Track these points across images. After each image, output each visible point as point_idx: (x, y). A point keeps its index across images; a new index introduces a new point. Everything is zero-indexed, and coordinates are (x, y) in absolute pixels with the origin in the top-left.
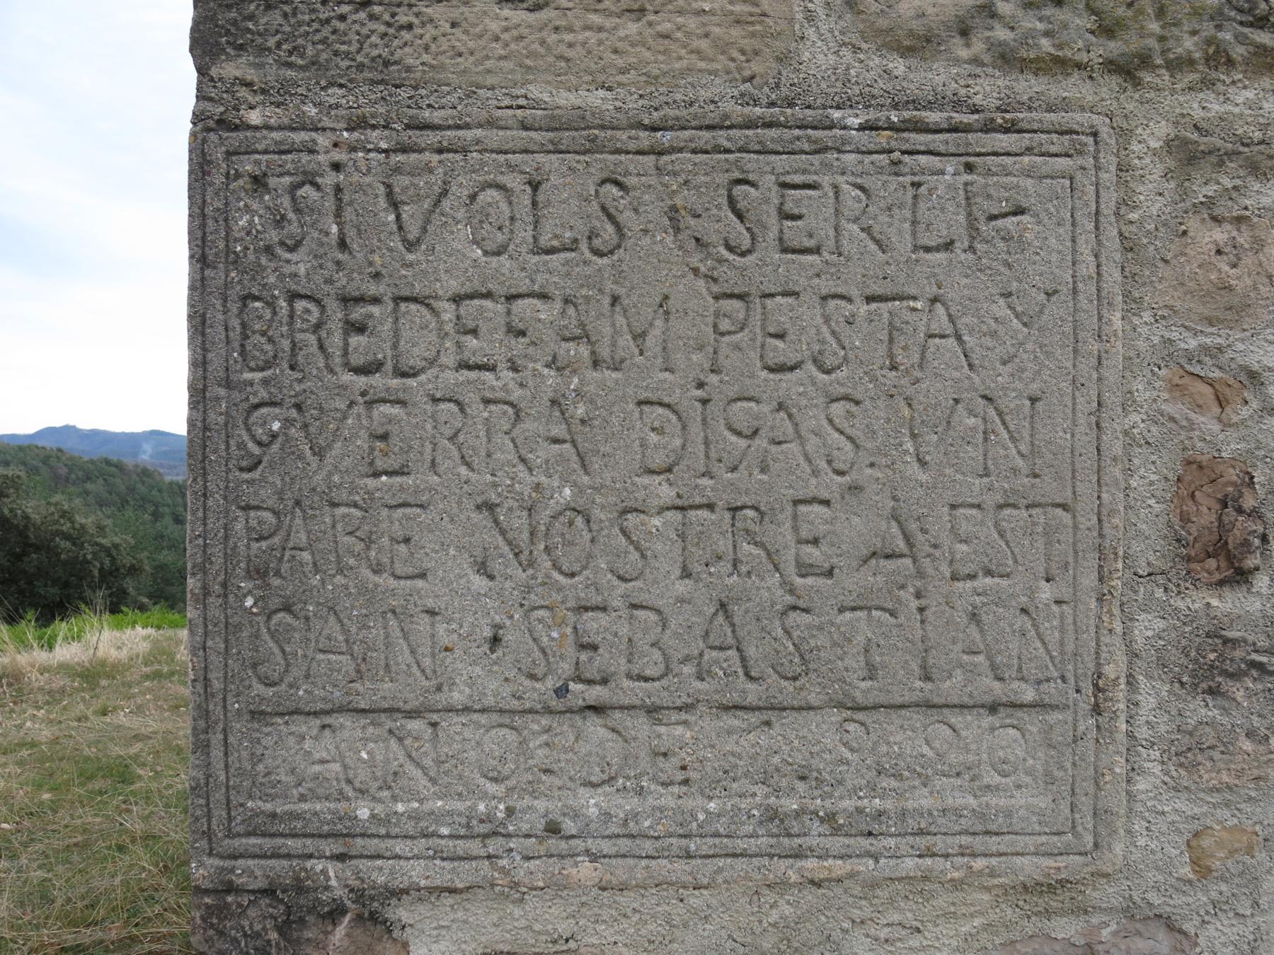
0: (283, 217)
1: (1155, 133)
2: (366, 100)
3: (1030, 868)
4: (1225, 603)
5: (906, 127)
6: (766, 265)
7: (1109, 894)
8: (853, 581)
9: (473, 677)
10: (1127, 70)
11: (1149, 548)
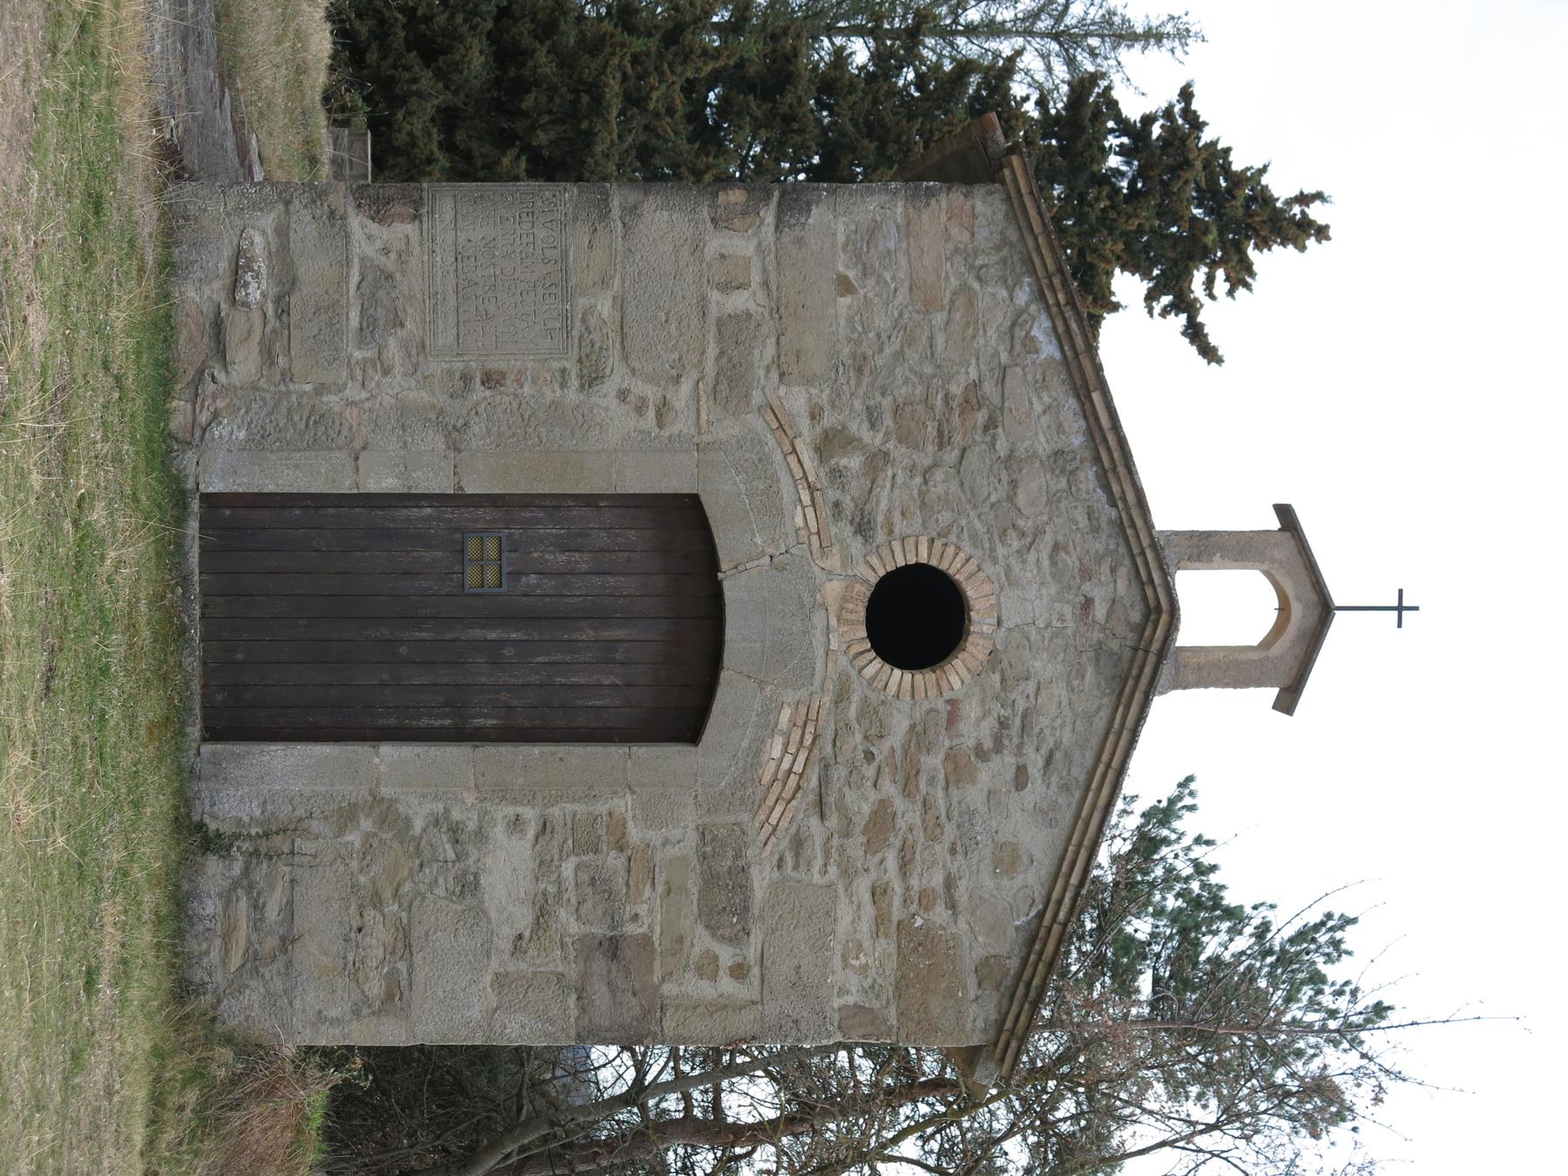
0: (104, 671)
1: (568, 365)
2: (570, 216)
3: (427, 342)
4: (478, 380)
5: (567, 317)
6: (540, 291)
7: (421, 358)
8: (481, 308)
9: (462, 237)
10: (580, 361)
11: (488, 365)
